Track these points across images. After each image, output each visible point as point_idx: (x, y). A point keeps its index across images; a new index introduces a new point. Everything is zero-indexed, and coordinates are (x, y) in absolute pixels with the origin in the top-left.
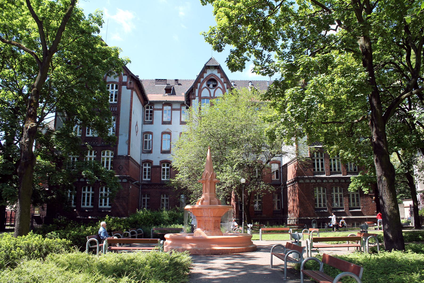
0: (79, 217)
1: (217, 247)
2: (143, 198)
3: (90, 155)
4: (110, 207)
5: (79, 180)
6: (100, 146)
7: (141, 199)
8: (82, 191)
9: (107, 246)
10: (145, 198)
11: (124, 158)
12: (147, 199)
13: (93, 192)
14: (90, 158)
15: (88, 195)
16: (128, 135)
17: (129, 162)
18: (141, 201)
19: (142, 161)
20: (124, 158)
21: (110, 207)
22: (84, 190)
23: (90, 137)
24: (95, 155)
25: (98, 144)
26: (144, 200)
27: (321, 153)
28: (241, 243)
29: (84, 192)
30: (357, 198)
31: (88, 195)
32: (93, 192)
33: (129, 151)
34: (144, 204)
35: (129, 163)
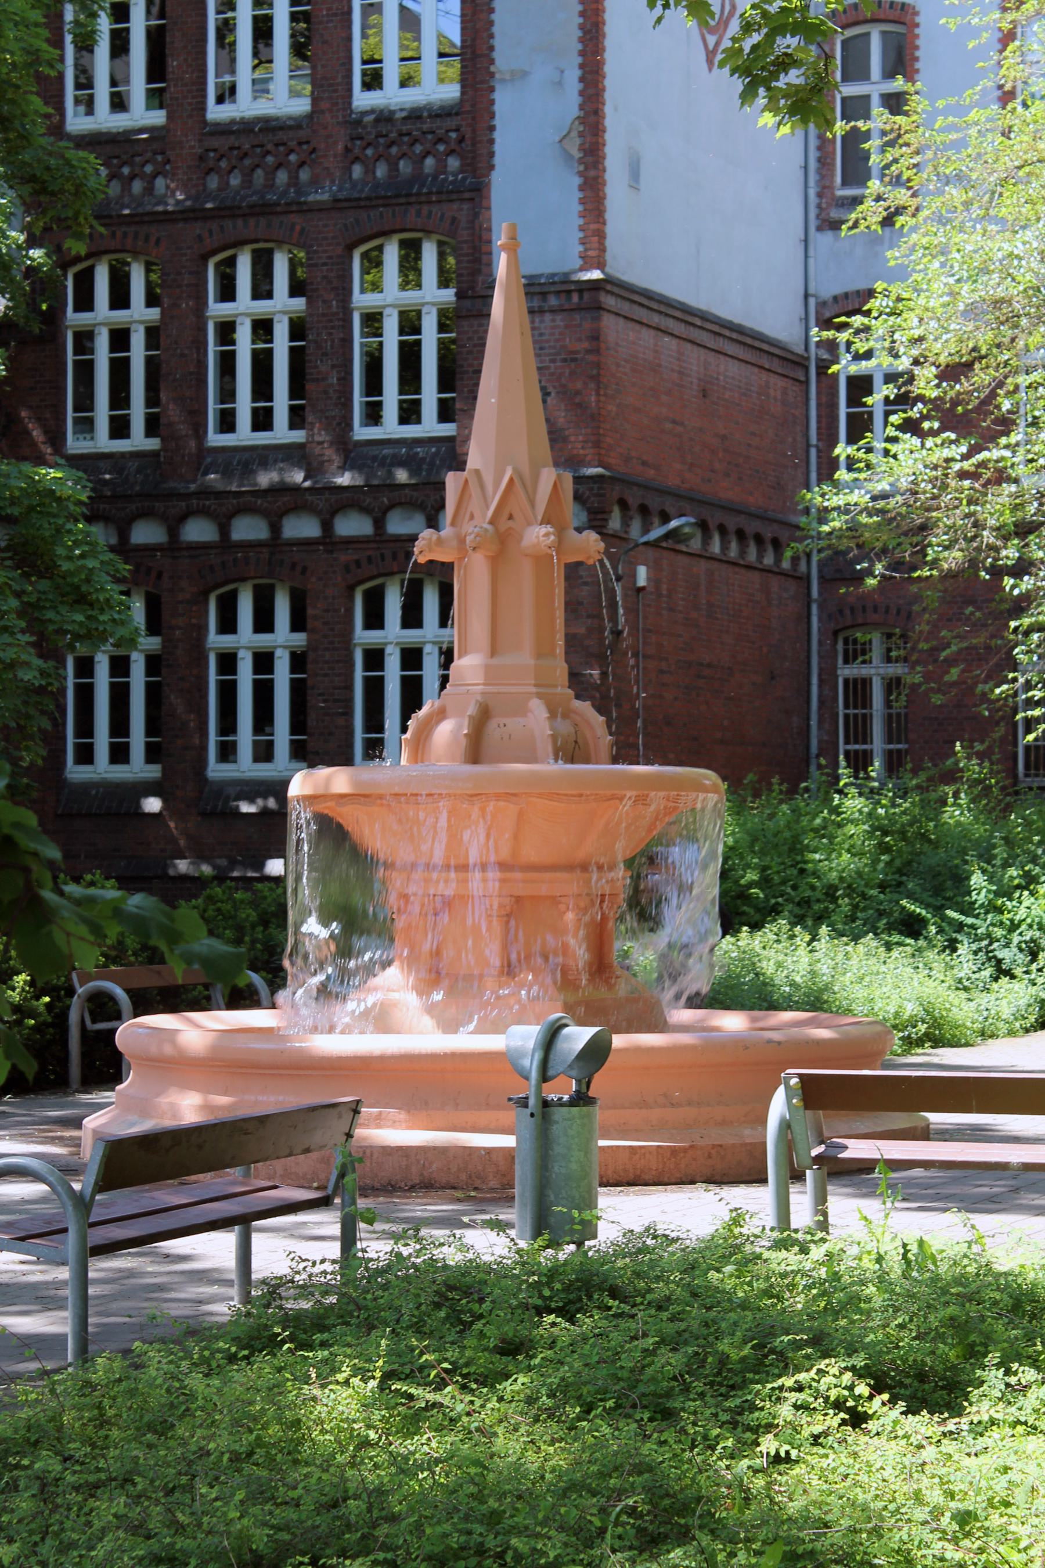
0: (183, 866)
1: (394, 1125)
2: (846, 672)
3: (404, 286)
4: (154, 772)
5: (173, 533)
6: (337, 205)
7: (828, 676)
8: (203, 629)
9: (802, 1132)
10: (865, 671)
11: (553, 301)
12: (892, 685)
13: (300, 639)
14: (402, 314)
15: (264, 661)
16: (573, 75)
17: (596, 337)
18: (827, 703)
19: (822, 305)
20: (553, 301)
21: (154, 772)
22: (375, 619)
23: (246, 127)
24: (444, 282)
25: (315, 182)
26: (859, 690)
27: (403, 244)
28: (644, 1104)
29: (226, 641)
30: (113, 686)
31: (264, 661)
32: (300, 639)
33: (601, 235)
34: (859, 730)
35: (597, 351)
